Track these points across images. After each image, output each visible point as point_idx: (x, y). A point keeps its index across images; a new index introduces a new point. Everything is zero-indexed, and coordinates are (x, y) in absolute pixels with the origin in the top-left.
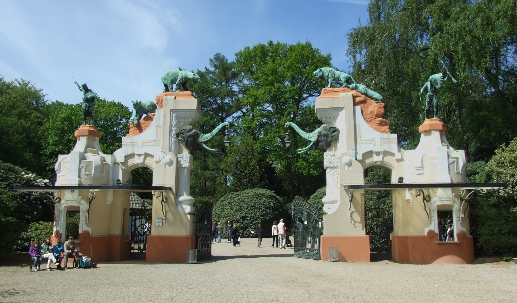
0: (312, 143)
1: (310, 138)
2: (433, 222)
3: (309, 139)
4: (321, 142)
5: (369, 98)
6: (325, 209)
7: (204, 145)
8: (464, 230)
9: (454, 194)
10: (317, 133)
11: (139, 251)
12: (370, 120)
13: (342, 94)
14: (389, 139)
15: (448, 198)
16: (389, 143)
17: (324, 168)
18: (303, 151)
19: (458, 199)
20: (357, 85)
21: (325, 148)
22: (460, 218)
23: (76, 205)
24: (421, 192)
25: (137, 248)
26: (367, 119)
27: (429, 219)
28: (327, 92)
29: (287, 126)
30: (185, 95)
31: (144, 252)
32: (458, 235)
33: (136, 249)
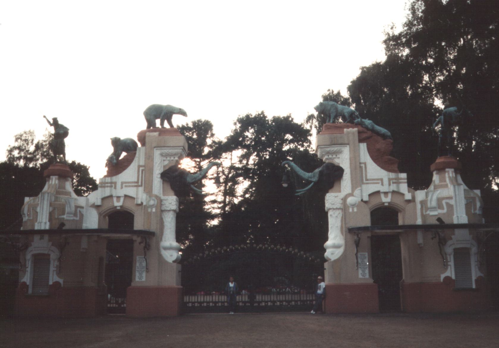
0: (312, 184)
2: (449, 267)
3: (310, 179)
7: (192, 186)
8: (482, 275)
11: (117, 306)
15: (463, 241)
17: (326, 209)
18: (301, 193)
20: (363, 120)
23: (46, 252)
25: (114, 302)
31: (122, 306)
32: (477, 281)
33: (113, 303)
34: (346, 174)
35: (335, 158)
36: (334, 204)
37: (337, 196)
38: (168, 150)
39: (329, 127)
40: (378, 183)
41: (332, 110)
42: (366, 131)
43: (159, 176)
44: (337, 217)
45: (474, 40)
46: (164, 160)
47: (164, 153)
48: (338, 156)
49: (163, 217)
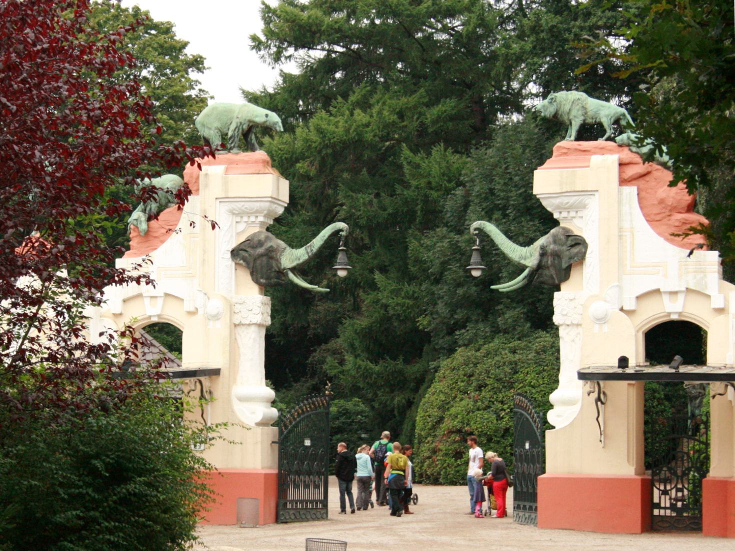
1: (525, 259)
3: (523, 262)
4: (548, 268)
5: (659, 167)
6: (551, 417)
10: (538, 249)
11: (674, 514)
12: (658, 218)
13: (595, 159)
21: (557, 282)
25: (668, 505)
26: (653, 217)
27: (602, 439)
28: (567, 152)
29: (476, 229)
30: (246, 162)
33: (665, 508)
35: (574, 217)
36: (566, 315)
38: (243, 204)
41: (574, 113)
43: (229, 255)
45: (541, 90)
47: (234, 209)
48: (580, 214)
49: (238, 337)
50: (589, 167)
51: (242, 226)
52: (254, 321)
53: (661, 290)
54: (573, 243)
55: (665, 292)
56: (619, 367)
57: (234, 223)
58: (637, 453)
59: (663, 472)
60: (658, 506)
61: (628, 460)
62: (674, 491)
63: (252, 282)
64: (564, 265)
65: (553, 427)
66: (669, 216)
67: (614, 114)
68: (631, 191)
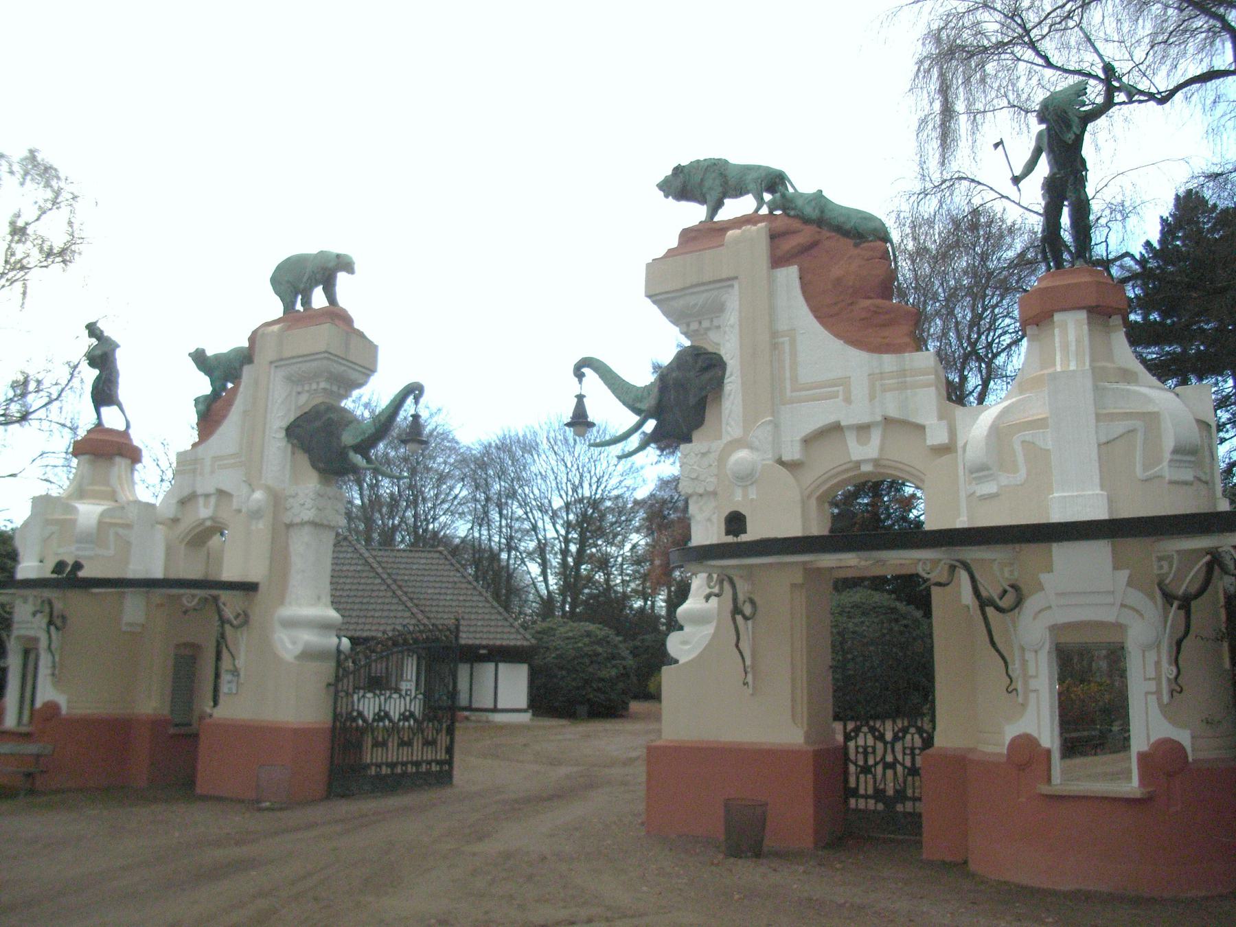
9: (1124, 575)
14: (902, 373)
16: (903, 387)
19: (1155, 603)
22: (1159, 684)
24: (726, 585)
25: (870, 791)
33: (866, 797)
34: (731, 375)
35: (708, 329)
36: (696, 479)
37: (709, 452)
38: (298, 365)
39: (693, 234)
40: (834, 396)
41: (708, 184)
42: (797, 224)
43: (283, 434)
44: (709, 520)
46: (299, 393)
48: (716, 323)
50: (723, 245)
51: (303, 398)
52: (306, 518)
53: (843, 424)
54: (704, 365)
55: (850, 427)
56: (728, 533)
57: (294, 394)
58: (1051, 707)
59: (861, 735)
60: (854, 793)
61: (793, 716)
62: (880, 768)
63: (311, 467)
64: (692, 401)
65: (676, 662)
66: (852, 304)
67: (766, 176)
68: (790, 274)
